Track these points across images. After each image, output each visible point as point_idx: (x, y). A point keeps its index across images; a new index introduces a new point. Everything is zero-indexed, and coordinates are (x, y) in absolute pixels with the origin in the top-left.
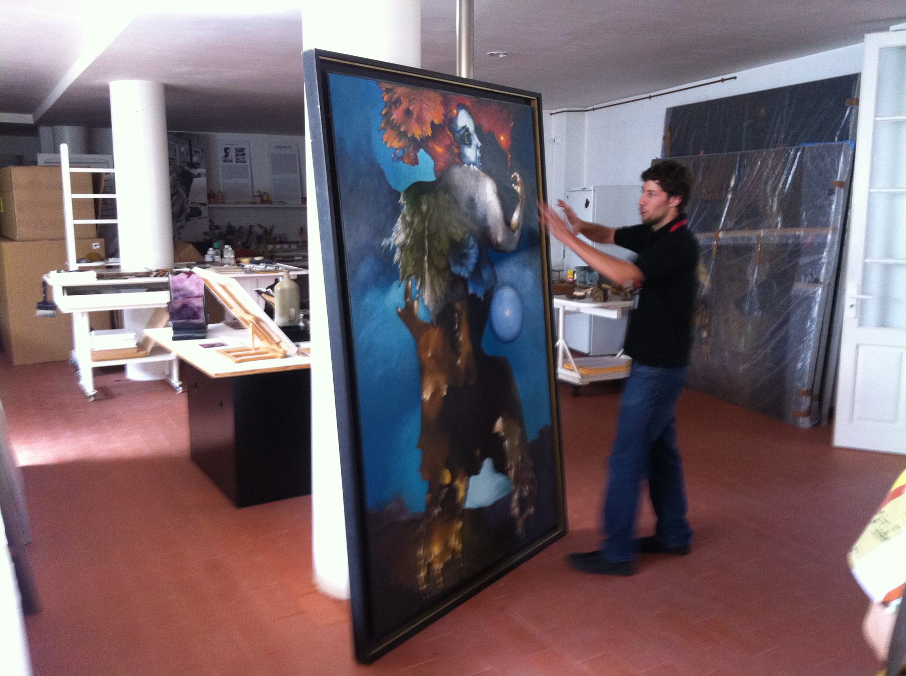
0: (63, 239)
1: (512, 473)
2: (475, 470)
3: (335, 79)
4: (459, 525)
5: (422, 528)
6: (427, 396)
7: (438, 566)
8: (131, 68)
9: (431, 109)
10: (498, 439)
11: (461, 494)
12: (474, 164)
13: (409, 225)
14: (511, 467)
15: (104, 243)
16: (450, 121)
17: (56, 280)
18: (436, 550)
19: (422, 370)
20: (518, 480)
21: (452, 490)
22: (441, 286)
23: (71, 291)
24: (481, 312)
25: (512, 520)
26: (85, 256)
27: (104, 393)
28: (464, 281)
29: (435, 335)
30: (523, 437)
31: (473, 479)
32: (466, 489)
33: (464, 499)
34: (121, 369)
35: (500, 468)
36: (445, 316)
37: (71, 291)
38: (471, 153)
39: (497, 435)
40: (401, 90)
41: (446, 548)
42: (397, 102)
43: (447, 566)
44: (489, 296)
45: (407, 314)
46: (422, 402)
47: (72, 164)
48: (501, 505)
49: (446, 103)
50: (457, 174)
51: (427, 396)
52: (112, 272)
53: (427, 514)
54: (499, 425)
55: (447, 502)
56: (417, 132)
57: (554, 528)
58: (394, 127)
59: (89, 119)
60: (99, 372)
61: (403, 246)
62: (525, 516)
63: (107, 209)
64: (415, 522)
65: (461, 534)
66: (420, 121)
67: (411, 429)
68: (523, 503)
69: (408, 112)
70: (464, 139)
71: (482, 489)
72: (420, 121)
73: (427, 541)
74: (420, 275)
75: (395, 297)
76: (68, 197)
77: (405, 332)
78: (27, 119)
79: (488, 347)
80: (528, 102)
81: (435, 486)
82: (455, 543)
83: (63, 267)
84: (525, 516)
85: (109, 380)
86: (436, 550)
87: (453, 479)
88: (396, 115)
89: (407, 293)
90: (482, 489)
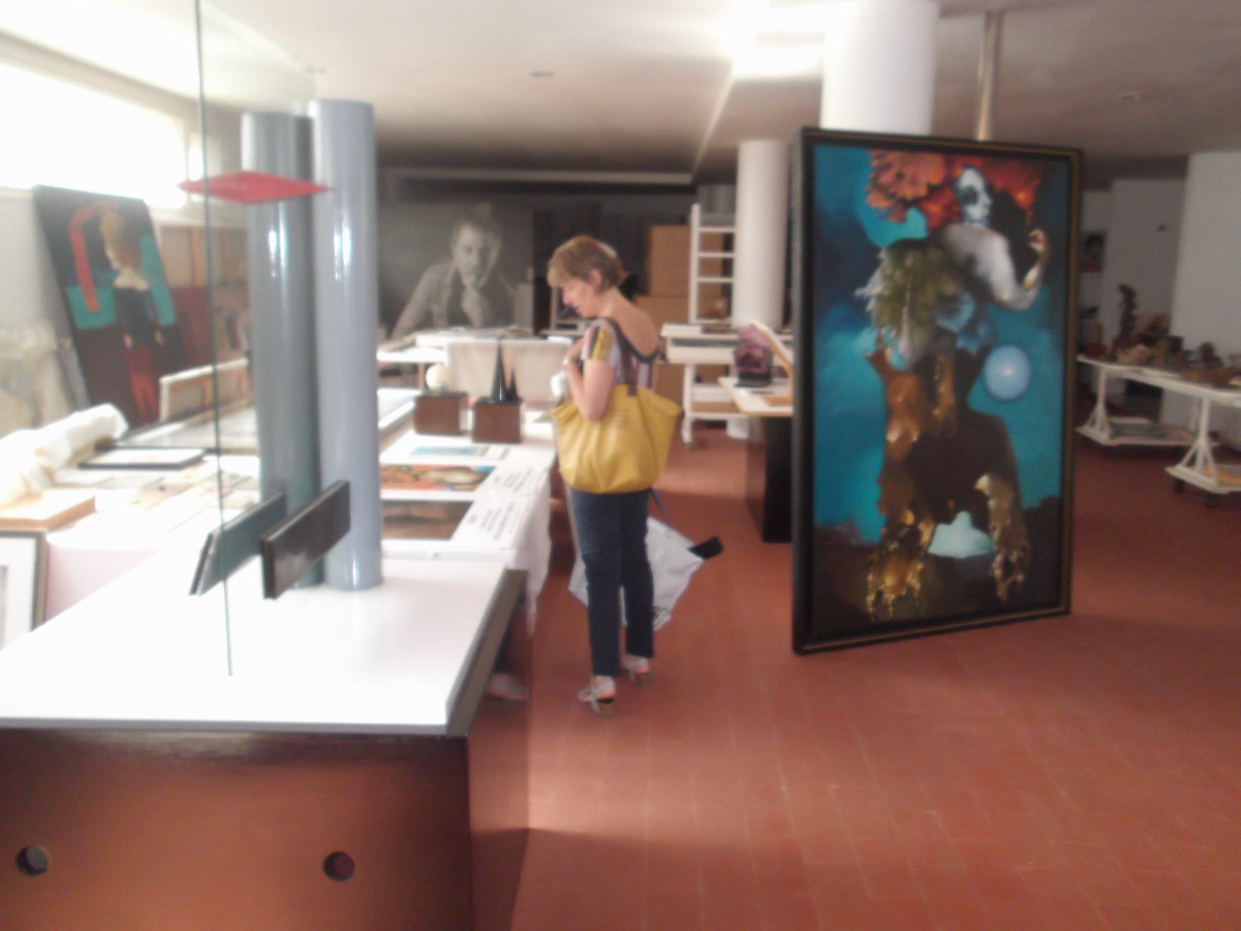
0: (684, 296)
1: (996, 535)
2: (947, 518)
3: (821, 152)
4: (920, 566)
5: (874, 556)
6: (893, 436)
7: (890, 597)
8: (757, 131)
9: (929, 171)
10: (981, 498)
11: (925, 538)
12: (979, 221)
13: (889, 278)
14: (994, 529)
15: (719, 302)
16: (950, 182)
17: (670, 331)
18: (889, 581)
19: (889, 413)
20: (1005, 542)
21: (915, 533)
22: (921, 338)
23: (680, 342)
24: (970, 369)
25: (992, 583)
26: (707, 312)
27: (700, 444)
28: (952, 336)
29: (908, 385)
30: (1017, 501)
31: (942, 529)
32: (933, 534)
33: (930, 543)
34: (721, 425)
35: (981, 522)
36: (924, 367)
37: (680, 342)
38: (978, 211)
39: (980, 493)
40: (893, 156)
41: (902, 582)
42: (888, 167)
43: (900, 599)
44: (985, 352)
45: (878, 360)
46: (887, 443)
47: (704, 223)
48: (979, 563)
49: (949, 164)
50: (956, 232)
51: (893, 436)
52: (727, 329)
53: (883, 545)
54: (983, 483)
55: (911, 546)
56: (908, 192)
57: (1056, 604)
60: (699, 425)
61: (880, 298)
62: (1010, 580)
63: (727, 267)
64: (866, 550)
65: (922, 575)
66: (914, 182)
67: (873, 465)
68: (1008, 567)
69: (900, 176)
70: (971, 196)
71: (956, 539)
72: (914, 182)
73: (880, 569)
74: (896, 322)
75: (865, 342)
76: (696, 255)
77: (872, 376)
78: (684, 179)
79: (977, 401)
80: (1066, 159)
81: (893, 524)
82: (913, 581)
83: (682, 319)
84: (1010, 580)
85: (711, 435)
86: (889, 581)
87: (917, 521)
88: (886, 178)
89: (879, 340)
90: (956, 539)
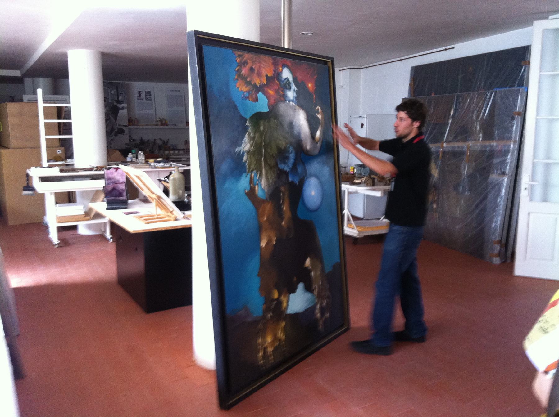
0: (39, 147)
1: (316, 292)
2: (293, 290)
3: (206, 49)
4: (283, 324)
5: (260, 326)
6: (263, 244)
7: (270, 349)
8: (81, 42)
9: (266, 67)
10: (307, 271)
11: (285, 305)
12: (293, 101)
13: (252, 139)
14: (315, 288)
15: (64, 150)
16: (278, 75)
17: (35, 173)
18: (269, 339)
19: (260, 229)
20: (320, 296)
21: (279, 303)
22: (272, 176)
23: (44, 179)
24: (297, 192)
25: (316, 321)
26: (53, 158)
27: (64, 243)
28: (286, 173)
29: (268, 207)
30: (323, 270)
31: (292, 296)
32: (288, 302)
33: (287, 308)
34: (75, 227)
35: (308, 288)
36: (274, 195)
37: (44, 179)
38: (291, 94)
39: (307, 268)
40: (247, 56)
41: (275, 338)
42: (245, 63)
43: (276, 349)
44: (302, 183)
45: (251, 194)
46: (261, 248)
47: (45, 101)
48: (309, 312)
49: (275, 64)
50: (282, 107)
51: (263, 244)
52: (69, 168)
53: (264, 317)
54: (308, 262)
55: (276, 310)
56: (257, 81)
57: (342, 326)
58: (243, 78)
60: (61, 230)
61: (249, 152)
62: (324, 318)
63: (66, 129)
64: (256, 322)
65: (285, 329)
66: (259, 74)
67: (254, 265)
68: (322, 310)
69: (252, 69)
70: (286, 86)
71: (298, 301)
72: (259, 74)
73: (264, 334)
74: (259, 170)
75: (244, 183)
76: (42, 121)
77: (250, 205)
78: (17, 73)
79: (301, 214)
80: (326, 63)
81: (268, 300)
82: (281, 335)
84: (324, 318)
85: (68, 235)
86: (269, 339)
87: (280, 295)
88: (245, 71)
89: (251, 181)
90: (298, 301)
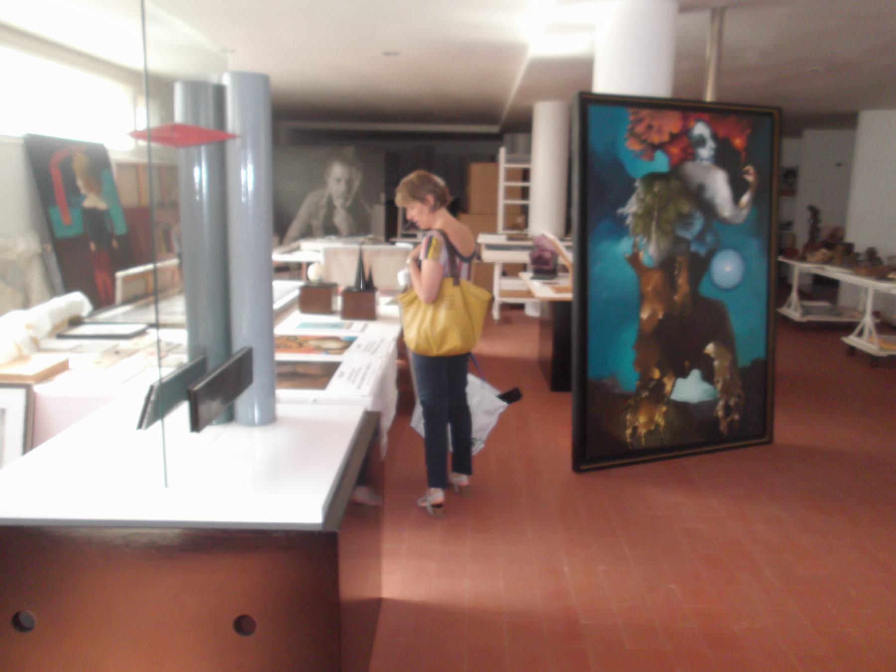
0: (494, 214)
1: (719, 386)
2: (684, 374)
4: (664, 409)
5: (631, 402)
6: (645, 315)
7: (642, 431)
8: (546, 94)
9: (671, 123)
10: (709, 360)
11: (668, 388)
12: (707, 160)
13: (642, 201)
14: (718, 382)
15: (519, 218)
16: (686, 131)
17: (484, 239)
18: (642, 419)
19: (642, 298)
20: (726, 391)
21: (660, 385)
22: (665, 244)
23: (491, 247)
24: (700, 266)
25: (716, 421)
26: (511, 225)
27: (505, 320)
28: (687, 242)
29: (656, 278)
30: (734, 362)
31: (680, 382)
32: (674, 386)
33: (671, 392)
34: (521, 307)
35: (708, 377)
36: (667, 265)
37: (491, 247)
38: (706, 152)
39: (708, 356)
40: (645, 113)
41: (651, 420)
42: (641, 120)
43: (650, 433)
44: (711, 254)
45: (634, 260)
46: (640, 320)
47: (508, 161)
48: (707, 407)
49: (685, 119)
50: (690, 168)
51: (645, 315)
52: (525, 238)
53: (637, 393)
54: (710, 348)
55: (658, 394)
56: (656, 139)
57: (763, 436)
58: (633, 135)
59: (520, 125)
60: (505, 307)
61: (635, 215)
62: (729, 419)
63: (525, 193)
64: (625, 397)
65: (666, 415)
66: (660, 131)
67: (630, 335)
68: (728, 409)
69: (650, 127)
70: (701, 142)
71: (690, 389)
72: (660, 131)
73: (636, 411)
74: (647, 233)
75: (625, 247)
76: (502, 184)
77: (630, 272)
78: (494, 129)
79: (705, 290)
80: (770, 115)
81: (645, 378)
82: (659, 419)
83: (493, 230)
84: (729, 419)
85: (513, 314)
86: (642, 419)
87: (662, 376)
88: (640, 129)
89: (635, 245)
90: (690, 389)
